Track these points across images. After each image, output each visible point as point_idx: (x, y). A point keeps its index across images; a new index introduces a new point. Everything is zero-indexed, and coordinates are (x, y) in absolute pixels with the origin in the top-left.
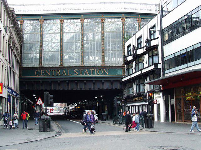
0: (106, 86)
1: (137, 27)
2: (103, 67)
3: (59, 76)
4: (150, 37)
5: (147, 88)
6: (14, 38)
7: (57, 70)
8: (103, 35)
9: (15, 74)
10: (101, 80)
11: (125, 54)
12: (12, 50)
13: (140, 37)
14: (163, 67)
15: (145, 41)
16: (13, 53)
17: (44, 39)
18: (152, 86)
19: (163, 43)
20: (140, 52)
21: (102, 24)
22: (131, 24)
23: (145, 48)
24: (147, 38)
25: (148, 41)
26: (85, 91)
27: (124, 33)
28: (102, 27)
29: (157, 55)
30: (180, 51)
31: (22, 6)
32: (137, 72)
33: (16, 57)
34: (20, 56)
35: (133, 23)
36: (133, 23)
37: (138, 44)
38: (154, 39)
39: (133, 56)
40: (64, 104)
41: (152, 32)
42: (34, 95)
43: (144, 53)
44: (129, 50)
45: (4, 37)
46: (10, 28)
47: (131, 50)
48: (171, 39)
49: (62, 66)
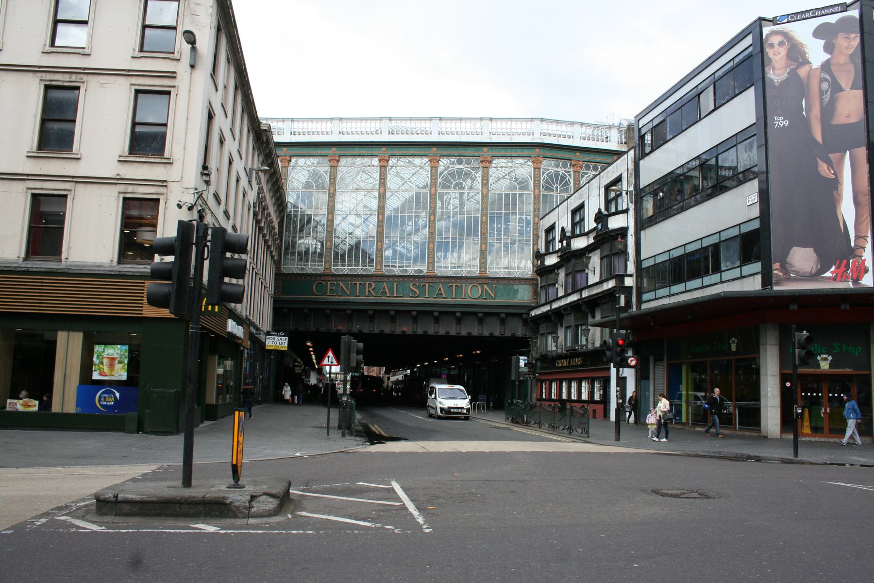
0: (492, 329)
1: (572, 181)
2: (482, 279)
3: (372, 299)
4: (607, 208)
5: (593, 335)
6: (266, 199)
7: (367, 283)
8: (485, 197)
9: (266, 289)
10: (432, 312)
11: (540, 247)
12: (261, 229)
13: (581, 207)
14: (639, 285)
15: (593, 218)
16: (263, 236)
17: (338, 206)
18: (607, 330)
19: (642, 224)
20: (579, 244)
21: (483, 171)
22: (557, 174)
23: (594, 234)
24: (600, 209)
25: (601, 218)
26: (436, 338)
27: (539, 197)
28: (483, 179)
29: (624, 252)
30: (685, 245)
31: (577, 127)
32: (569, 295)
33: (269, 247)
34: (278, 244)
35: (561, 171)
36: (561, 171)
37: (574, 225)
38: (617, 213)
39: (559, 254)
40: (375, 368)
41: (612, 195)
42: (309, 344)
43: (590, 249)
44: (551, 238)
45: (244, 196)
46: (260, 173)
47: (554, 239)
48: (663, 213)
49: (381, 273)
